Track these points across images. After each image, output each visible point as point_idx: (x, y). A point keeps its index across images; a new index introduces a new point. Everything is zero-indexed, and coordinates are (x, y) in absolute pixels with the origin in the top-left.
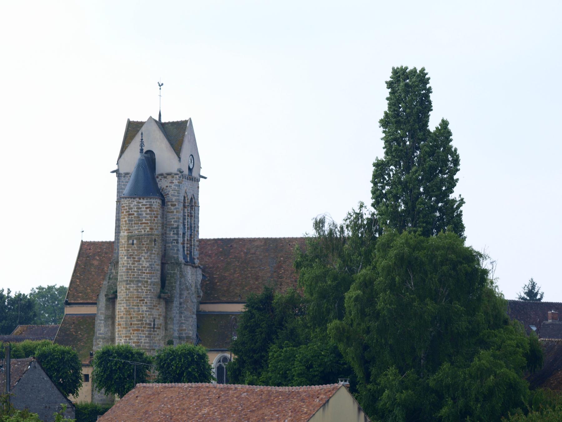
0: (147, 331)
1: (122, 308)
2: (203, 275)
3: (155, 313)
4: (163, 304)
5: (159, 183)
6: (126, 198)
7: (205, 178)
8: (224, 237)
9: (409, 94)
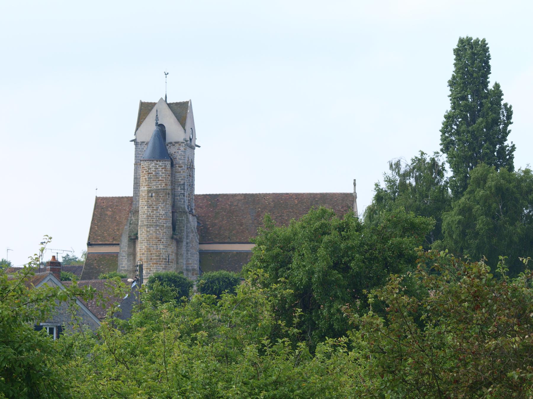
0: (164, 264)
1: (144, 247)
2: (198, 222)
3: (170, 250)
4: (174, 243)
5: (169, 150)
6: (146, 161)
7: (199, 147)
8: (211, 193)
9: (472, 59)
